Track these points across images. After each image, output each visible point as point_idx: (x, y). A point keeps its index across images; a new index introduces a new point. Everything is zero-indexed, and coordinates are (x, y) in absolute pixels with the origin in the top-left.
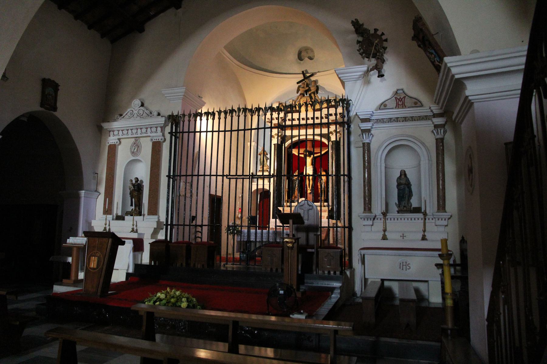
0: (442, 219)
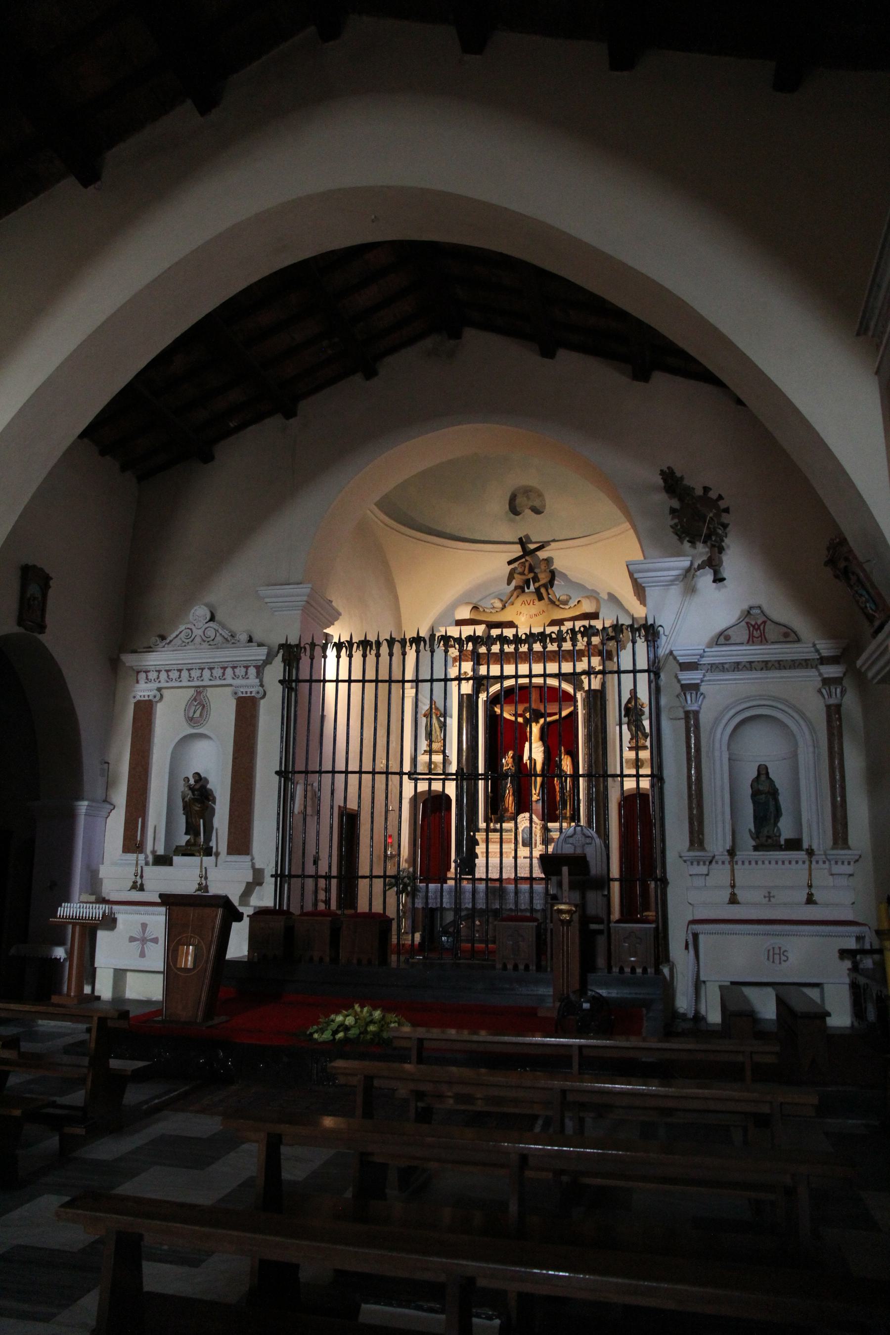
0: (843, 863)
